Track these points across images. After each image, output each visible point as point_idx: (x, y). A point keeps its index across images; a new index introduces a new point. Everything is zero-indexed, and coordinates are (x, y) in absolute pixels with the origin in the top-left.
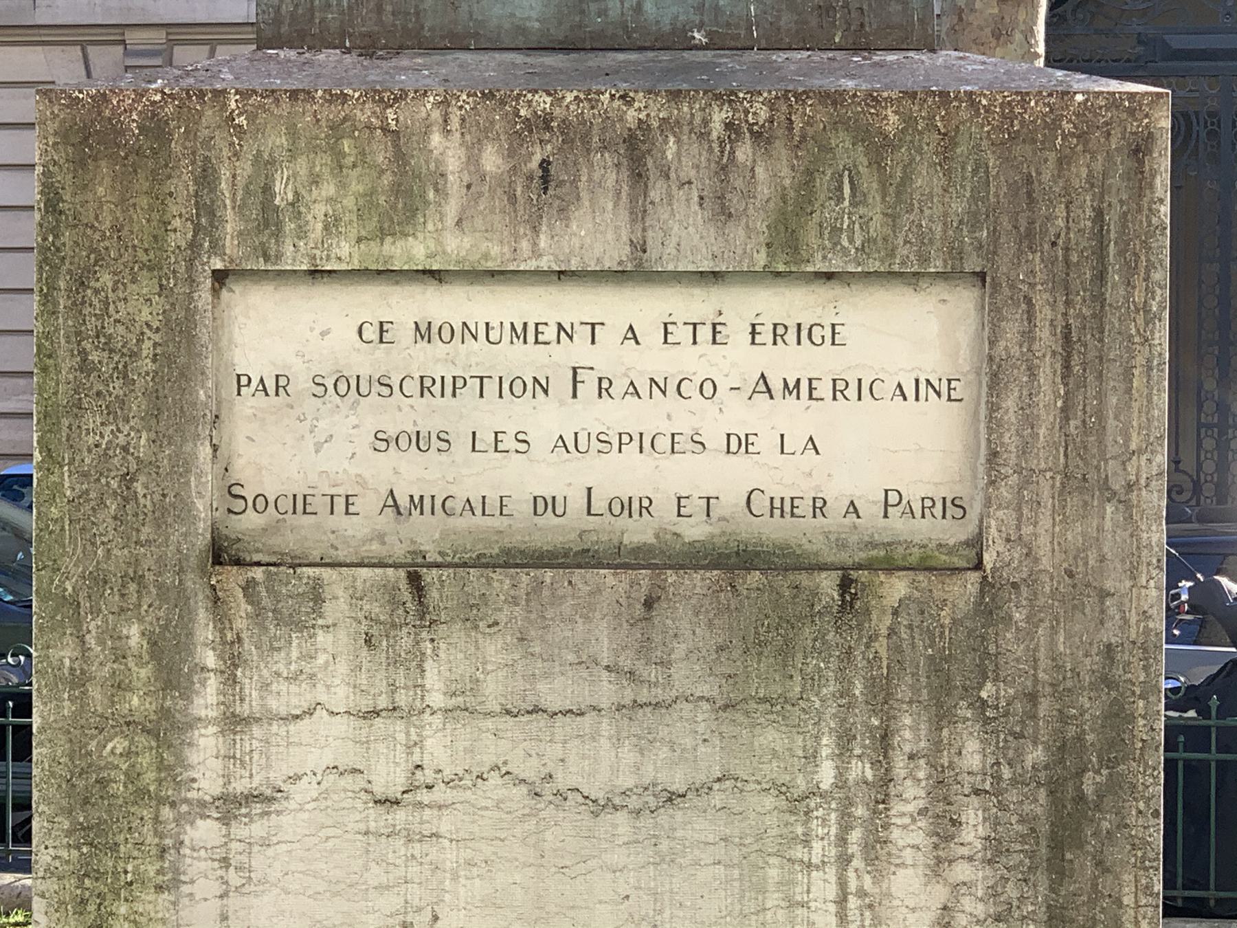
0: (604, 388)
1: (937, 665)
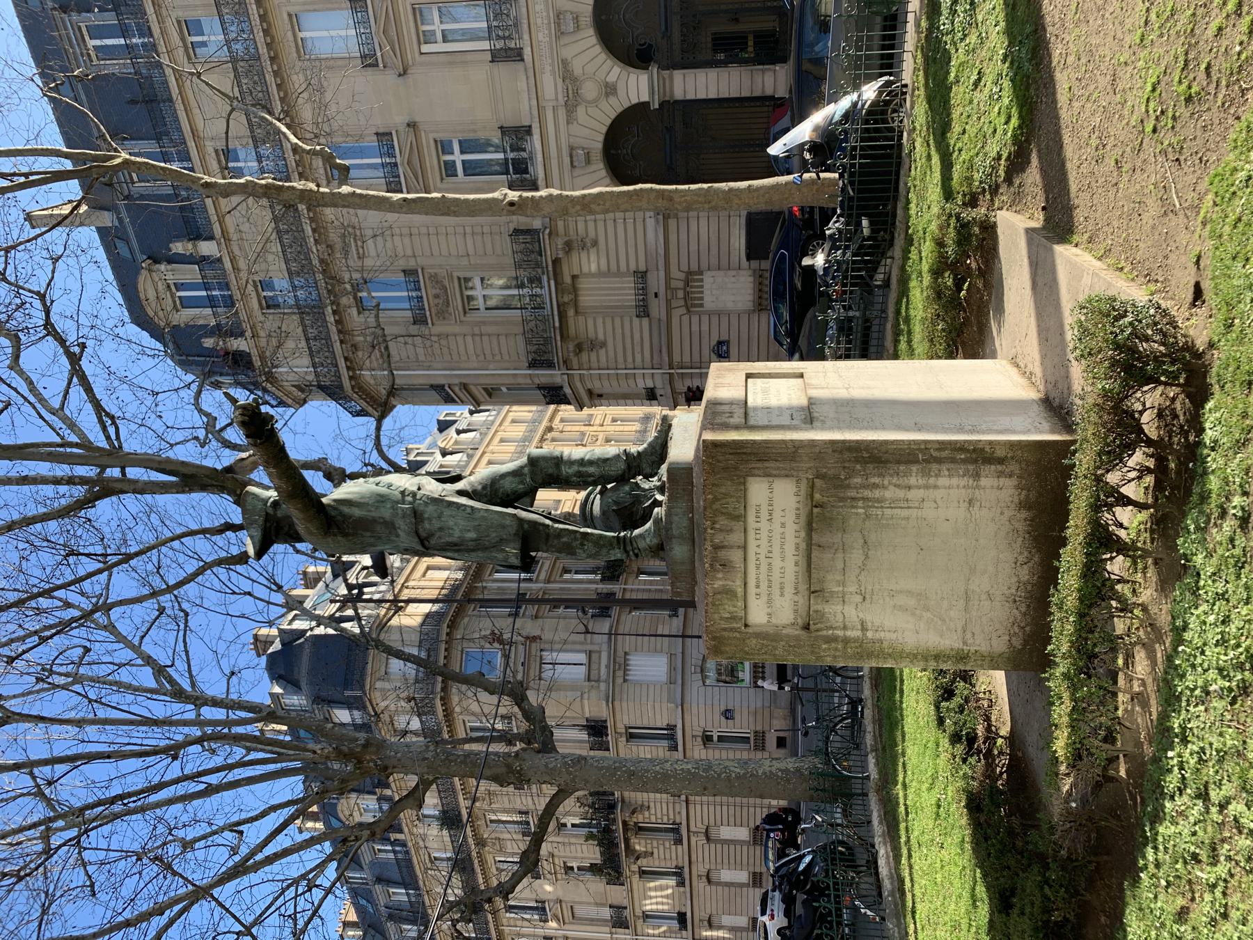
0: (770, 552)
1: (836, 487)
